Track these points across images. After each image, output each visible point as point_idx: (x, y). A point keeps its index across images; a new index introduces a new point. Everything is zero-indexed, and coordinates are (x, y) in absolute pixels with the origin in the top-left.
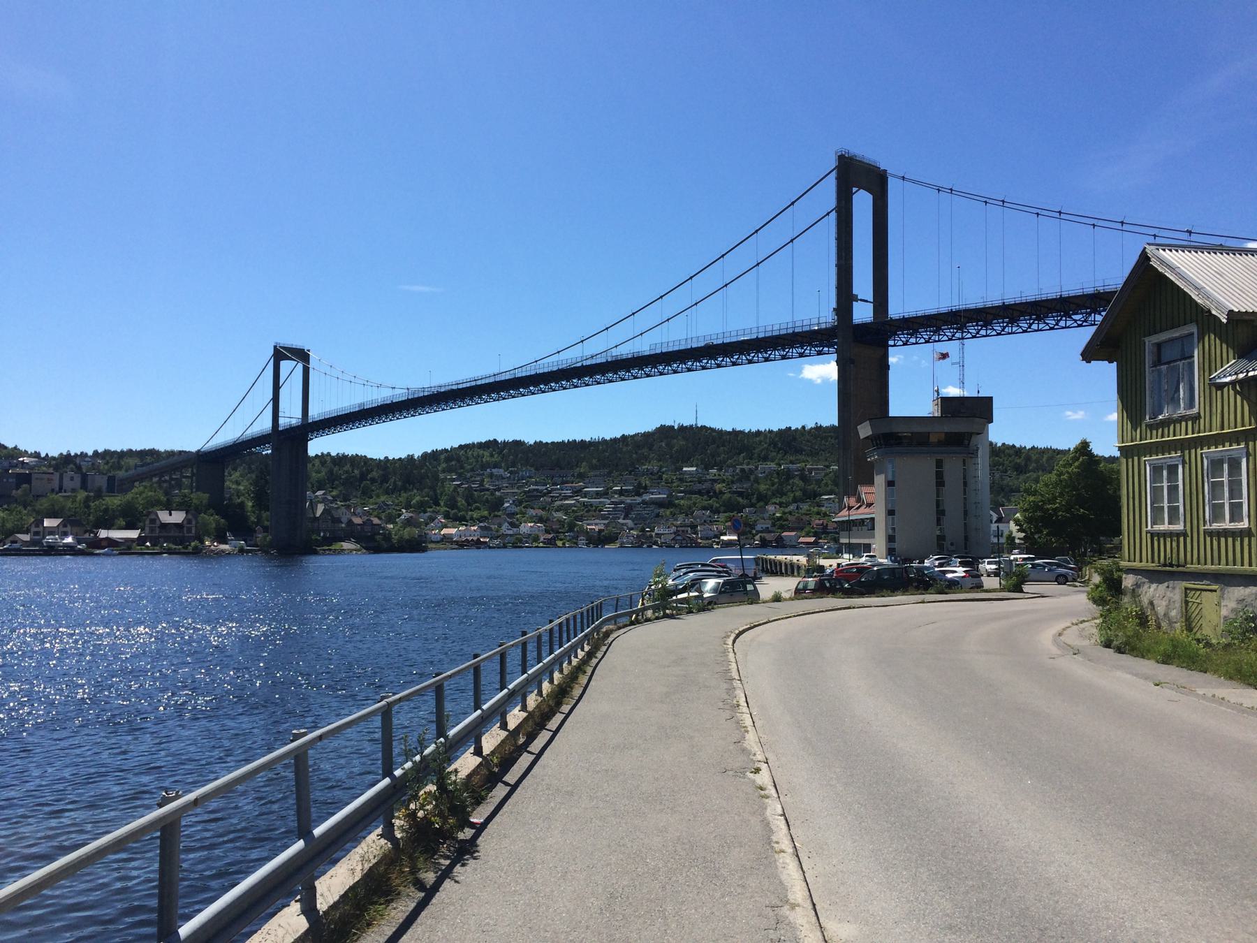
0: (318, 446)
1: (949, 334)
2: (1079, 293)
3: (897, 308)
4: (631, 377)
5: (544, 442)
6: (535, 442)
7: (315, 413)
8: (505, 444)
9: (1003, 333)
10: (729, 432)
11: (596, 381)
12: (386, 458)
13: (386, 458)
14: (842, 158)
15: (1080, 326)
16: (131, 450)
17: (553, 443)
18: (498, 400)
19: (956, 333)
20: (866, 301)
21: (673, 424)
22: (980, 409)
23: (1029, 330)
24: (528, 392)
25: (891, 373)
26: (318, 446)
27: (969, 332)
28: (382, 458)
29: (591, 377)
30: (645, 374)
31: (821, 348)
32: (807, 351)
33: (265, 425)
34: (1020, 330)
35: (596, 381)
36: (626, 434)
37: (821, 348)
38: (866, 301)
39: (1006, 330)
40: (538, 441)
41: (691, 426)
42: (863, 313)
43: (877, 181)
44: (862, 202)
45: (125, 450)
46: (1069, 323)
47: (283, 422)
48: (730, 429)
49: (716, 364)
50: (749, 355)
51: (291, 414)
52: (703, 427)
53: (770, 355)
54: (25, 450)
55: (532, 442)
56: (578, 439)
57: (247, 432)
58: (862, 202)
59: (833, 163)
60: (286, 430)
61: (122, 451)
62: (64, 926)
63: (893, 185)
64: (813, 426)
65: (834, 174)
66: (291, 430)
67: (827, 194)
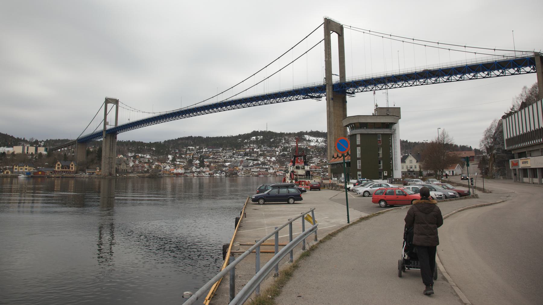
0: (122, 137)
1: (361, 89)
2: (414, 71)
3: (350, 77)
4: (237, 108)
5: (210, 137)
6: (207, 137)
7: (120, 124)
8: (195, 137)
9: (382, 89)
10: (279, 133)
11: (228, 109)
12: (150, 142)
13: (150, 142)
14: (325, 19)
15: (422, 84)
16: (59, 139)
17: (213, 137)
18: (189, 117)
19: (373, 87)
20: (337, 75)
21: (258, 130)
22: (395, 113)
23: (382, 89)
24: (213, 111)
25: (347, 104)
26: (122, 137)
27: (359, 89)
28: (149, 143)
29: (231, 106)
30: (248, 105)
31: (319, 94)
32: (299, 98)
33: (101, 128)
34: (369, 90)
35: (228, 109)
36: (241, 134)
37: (319, 94)
38: (337, 75)
39: (364, 90)
40: (208, 136)
41: (265, 131)
42: (336, 79)
43: (340, 31)
44: (334, 37)
45: (57, 139)
46: (397, 86)
47: (108, 127)
48: (280, 132)
49: (276, 101)
50: (283, 98)
51: (111, 125)
52: (269, 132)
53: (298, 97)
54: (17, 138)
55: (205, 137)
56: (223, 136)
57: (96, 131)
58: (334, 37)
59: (323, 21)
60: (109, 130)
61: (56, 140)
62: (257, 228)
63: (345, 31)
64: (310, 131)
65: (323, 26)
66: (111, 130)
67: (321, 32)
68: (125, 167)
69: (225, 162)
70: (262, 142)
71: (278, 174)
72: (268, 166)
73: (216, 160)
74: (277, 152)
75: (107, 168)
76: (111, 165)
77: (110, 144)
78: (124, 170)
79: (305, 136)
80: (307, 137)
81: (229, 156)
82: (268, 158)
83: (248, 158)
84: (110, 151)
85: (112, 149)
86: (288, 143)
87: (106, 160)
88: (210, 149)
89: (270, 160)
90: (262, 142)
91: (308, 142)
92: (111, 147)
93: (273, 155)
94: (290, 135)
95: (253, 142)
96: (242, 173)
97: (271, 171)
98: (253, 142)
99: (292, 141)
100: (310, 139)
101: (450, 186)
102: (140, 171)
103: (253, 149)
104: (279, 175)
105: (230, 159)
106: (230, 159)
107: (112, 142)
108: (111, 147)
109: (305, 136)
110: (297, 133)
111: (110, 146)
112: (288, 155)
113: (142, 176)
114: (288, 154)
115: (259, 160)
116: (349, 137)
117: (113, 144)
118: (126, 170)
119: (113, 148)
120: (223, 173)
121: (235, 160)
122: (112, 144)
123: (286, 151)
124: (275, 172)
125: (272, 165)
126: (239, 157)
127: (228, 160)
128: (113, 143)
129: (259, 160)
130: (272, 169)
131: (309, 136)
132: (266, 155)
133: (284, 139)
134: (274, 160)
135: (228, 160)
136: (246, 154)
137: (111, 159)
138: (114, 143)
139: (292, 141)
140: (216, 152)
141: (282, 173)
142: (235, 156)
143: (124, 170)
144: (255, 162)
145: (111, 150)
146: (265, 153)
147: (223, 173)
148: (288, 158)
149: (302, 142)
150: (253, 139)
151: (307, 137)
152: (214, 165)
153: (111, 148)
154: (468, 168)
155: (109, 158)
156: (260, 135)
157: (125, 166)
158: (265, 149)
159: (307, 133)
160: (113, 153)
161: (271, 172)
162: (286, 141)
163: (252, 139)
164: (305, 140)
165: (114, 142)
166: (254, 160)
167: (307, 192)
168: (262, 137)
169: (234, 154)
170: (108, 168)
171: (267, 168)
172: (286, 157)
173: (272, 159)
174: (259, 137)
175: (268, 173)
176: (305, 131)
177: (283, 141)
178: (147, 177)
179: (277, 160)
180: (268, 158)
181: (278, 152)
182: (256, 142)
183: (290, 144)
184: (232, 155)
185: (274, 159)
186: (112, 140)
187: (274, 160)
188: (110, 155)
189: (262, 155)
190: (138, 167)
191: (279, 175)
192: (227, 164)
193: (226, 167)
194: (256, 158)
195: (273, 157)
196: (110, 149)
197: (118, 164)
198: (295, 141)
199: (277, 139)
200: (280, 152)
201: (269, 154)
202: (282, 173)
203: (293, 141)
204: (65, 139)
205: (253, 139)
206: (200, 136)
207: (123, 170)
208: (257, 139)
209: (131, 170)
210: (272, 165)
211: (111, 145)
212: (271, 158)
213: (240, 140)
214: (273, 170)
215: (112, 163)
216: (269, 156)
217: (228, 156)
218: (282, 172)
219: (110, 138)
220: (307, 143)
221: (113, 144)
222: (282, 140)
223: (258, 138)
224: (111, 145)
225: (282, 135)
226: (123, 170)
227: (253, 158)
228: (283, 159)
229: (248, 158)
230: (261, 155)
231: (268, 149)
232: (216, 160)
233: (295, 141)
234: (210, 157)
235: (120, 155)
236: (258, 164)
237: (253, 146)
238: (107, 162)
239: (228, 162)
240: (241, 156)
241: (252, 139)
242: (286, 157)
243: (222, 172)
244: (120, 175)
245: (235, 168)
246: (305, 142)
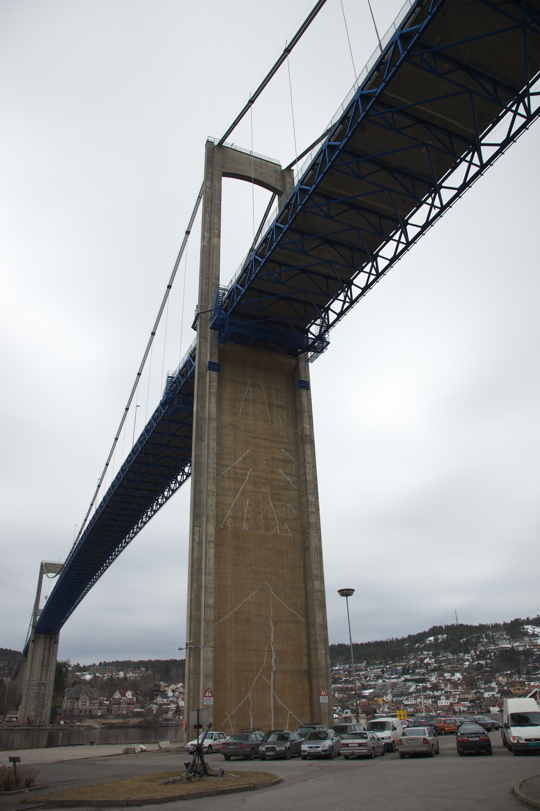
17: (362, 644)
68: (88, 704)
69: (365, 688)
70: (446, 646)
71: (456, 708)
72: (440, 692)
73: (348, 685)
74: (467, 661)
75: (32, 706)
76: (40, 700)
77: (44, 655)
78: (86, 711)
79: (525, 627)
80: (530, 629)
81: (375, 676)
82: (447, 675)
83: (408, 677)
84: (42, 669)
85: (48, 666)
86: (494, 643)
87: (32, 689)
88: (346, 666)
89: (451, 679)
90: (446, 646)
91: (533, 638)
92: (46, 660)
93: (456, 669)
94: (496, 627)
95: (428, 647)
96: (386, 710)
97: (443, 702)
98: (428, 647)
99: (501, 639)
100: (536, 633)
101: (52, 673)
102: (125, 712)
103: (422, 660)
104: (459, 710)
105: (373, 683)
106: (373, 683)
107: (47, 651)
108: (46, 660)
109: (525, 626)
110: (510, 624)
111: (43, 659)
112: (486, 667)
113: (122, 723)
114: (486, 663)
115: (429, 681)
116: (231, 520)
117: (49, 655)
118: (90, 711)
119: (49, 664)
120: (347, 710)
121: (384, 683)
122: (47, 654)
123: (484, 658)
124: (452, 704)
125: (450, 688)
126: (393, 676)
127: (371, 683)
128: (49, 652)
129: (429, 681)
130: (445, 697)
131: (534, 627)
132: (443, 669)
133: (486, 635)
134: (459, 679)
135: (371, 683)
136: (405, 671)
137: (42, 688)
138: (51, 653)
139: (501, 639)
140: (356, 670)
141: (464, 706)
142: (386, 675)
143: (86, 711)
144: (420, 684)
145: (45, 668)
146: (443, 666)
147: (347, 710)
148: (487, 672)
149: (522, 638)
150: (430, 640)
151: (530, 629)
152: (341, 695)
153: (45, 663)
154: (380, 222)
155: (39, 685)
156: (442, 634)
157: (88, 702)
158: (444, 658)
159: (528, 622)
160: (49, 675)
161: (444, 704)
162: (489, 639)
163: (427, 642)
164: (526, 634)
165: (52, 651)
166: (417, 681)
167: (182, 763)
168: (446, 635)
169: (383, 672)
170: (34, 708)
171: (435, 697)
172: (482, 671)
173: (455, 677)
174: (440, 636)
175: (438, 706)
176: (525, 618)
177: (485, 640)
178: (134, 727)
179: (464, 678)
180: (446, 675)
181: (469, 661)
182: (436, 648)
183: (498, 645)
184: (380, 673)
185: (458, 676)
186: (47, 646)
187: (459, 679)
188: (41, 679)
189: (436, 671)
190: (119, 704)
191: (459, 710)
192: (367, 692)
193: (365, 697)
194: (422, 677)
195: (457, 671)
196: (42, 667)
197: (73, 699)
198: (507, 639)
199: (472, 638)
200: (473, 661)
201: (449, 666)
202: (464, 706)
203: (504, 639)
204: (126, 660)
205: (429, 641)
206: (341, 643)
207: (83, 711)
208: (436, 640)
209: (103, 710)
210: (450, 688)
211: (46, 658)
212: (453, 675)
213: (407, 644)
214: (446, 699)
215: (44, 695)
216: (448, 672)
217: (372, 675)
218: (466, 703)
219: (45, 643)
220: (530, 640)
221: (49, 655)
222: (483, 638)
223: (439, 639)
224: (46, 658)
225: (482, 628)
226: (83, 711)
227: (417, 677)
228: (477, 675)
229: (408, 677)
230: (434, 670)
231: (451, 656)
232: (348, 685)
233: (507, 639)
234: (341, 679)
235: (161, 682)
236: (425, 689)
237: (428, 653)
238: (34, 694)
239: (371, 688)
240: (396, 674)
241: (427, 642)
242: (482, 671)
243: (343, 710)
244: (68, 722)
245: (376, 699)
246: (526, 639)
